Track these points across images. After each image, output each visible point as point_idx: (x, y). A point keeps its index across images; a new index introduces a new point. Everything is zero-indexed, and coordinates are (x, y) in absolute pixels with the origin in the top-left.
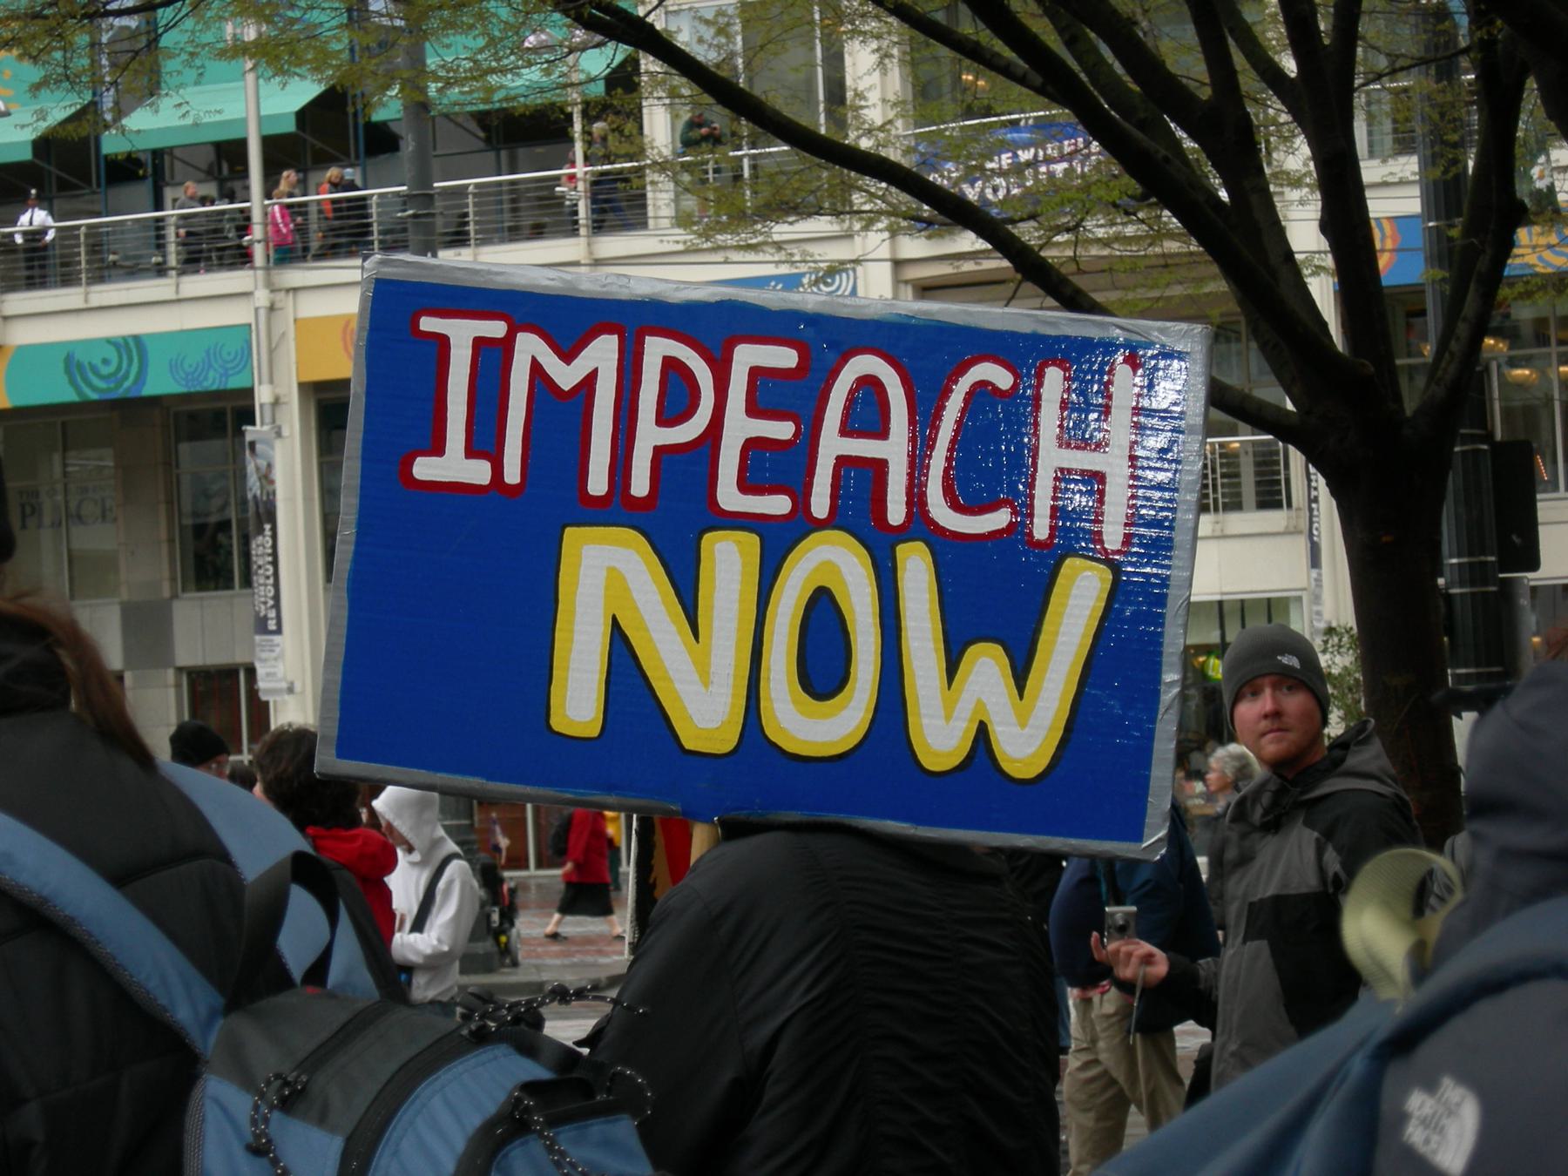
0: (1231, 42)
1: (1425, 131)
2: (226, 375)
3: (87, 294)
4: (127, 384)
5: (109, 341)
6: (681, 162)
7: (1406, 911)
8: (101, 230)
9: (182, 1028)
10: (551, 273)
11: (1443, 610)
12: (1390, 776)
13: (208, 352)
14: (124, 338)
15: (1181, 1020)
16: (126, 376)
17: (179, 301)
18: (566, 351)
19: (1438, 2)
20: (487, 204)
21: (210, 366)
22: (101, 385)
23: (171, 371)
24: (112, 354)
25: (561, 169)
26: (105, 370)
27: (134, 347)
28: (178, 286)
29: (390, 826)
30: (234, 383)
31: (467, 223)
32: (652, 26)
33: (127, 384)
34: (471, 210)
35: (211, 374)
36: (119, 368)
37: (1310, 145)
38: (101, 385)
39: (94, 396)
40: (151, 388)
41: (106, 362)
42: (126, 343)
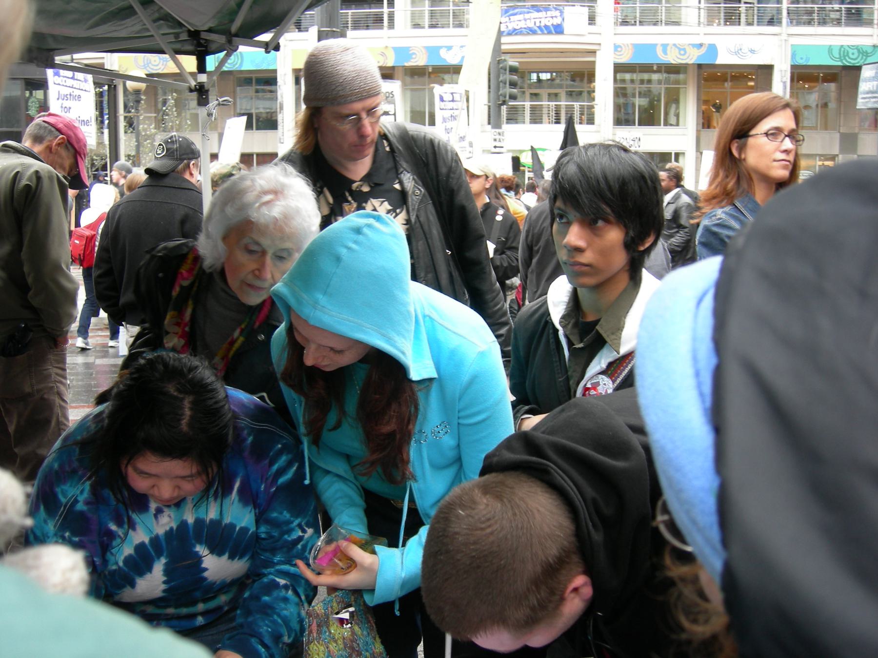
1: (257, 184)
2: (269, 65)
4: (237, 66)
6: (670, 4)
9: (744, 112)
10: (62, 47)
11: (647, 245)
12: (712, 208)
16: (236, 64)
19: (3, 269)
20: (345, 18)
23: (829, 52)
29: (566, 123)
30: (271, 68)
31: (348, 24)
33: (237, 66)
34: (350, 20)
35: (264, 65)
36: (234, 62)
37: (383, 643)
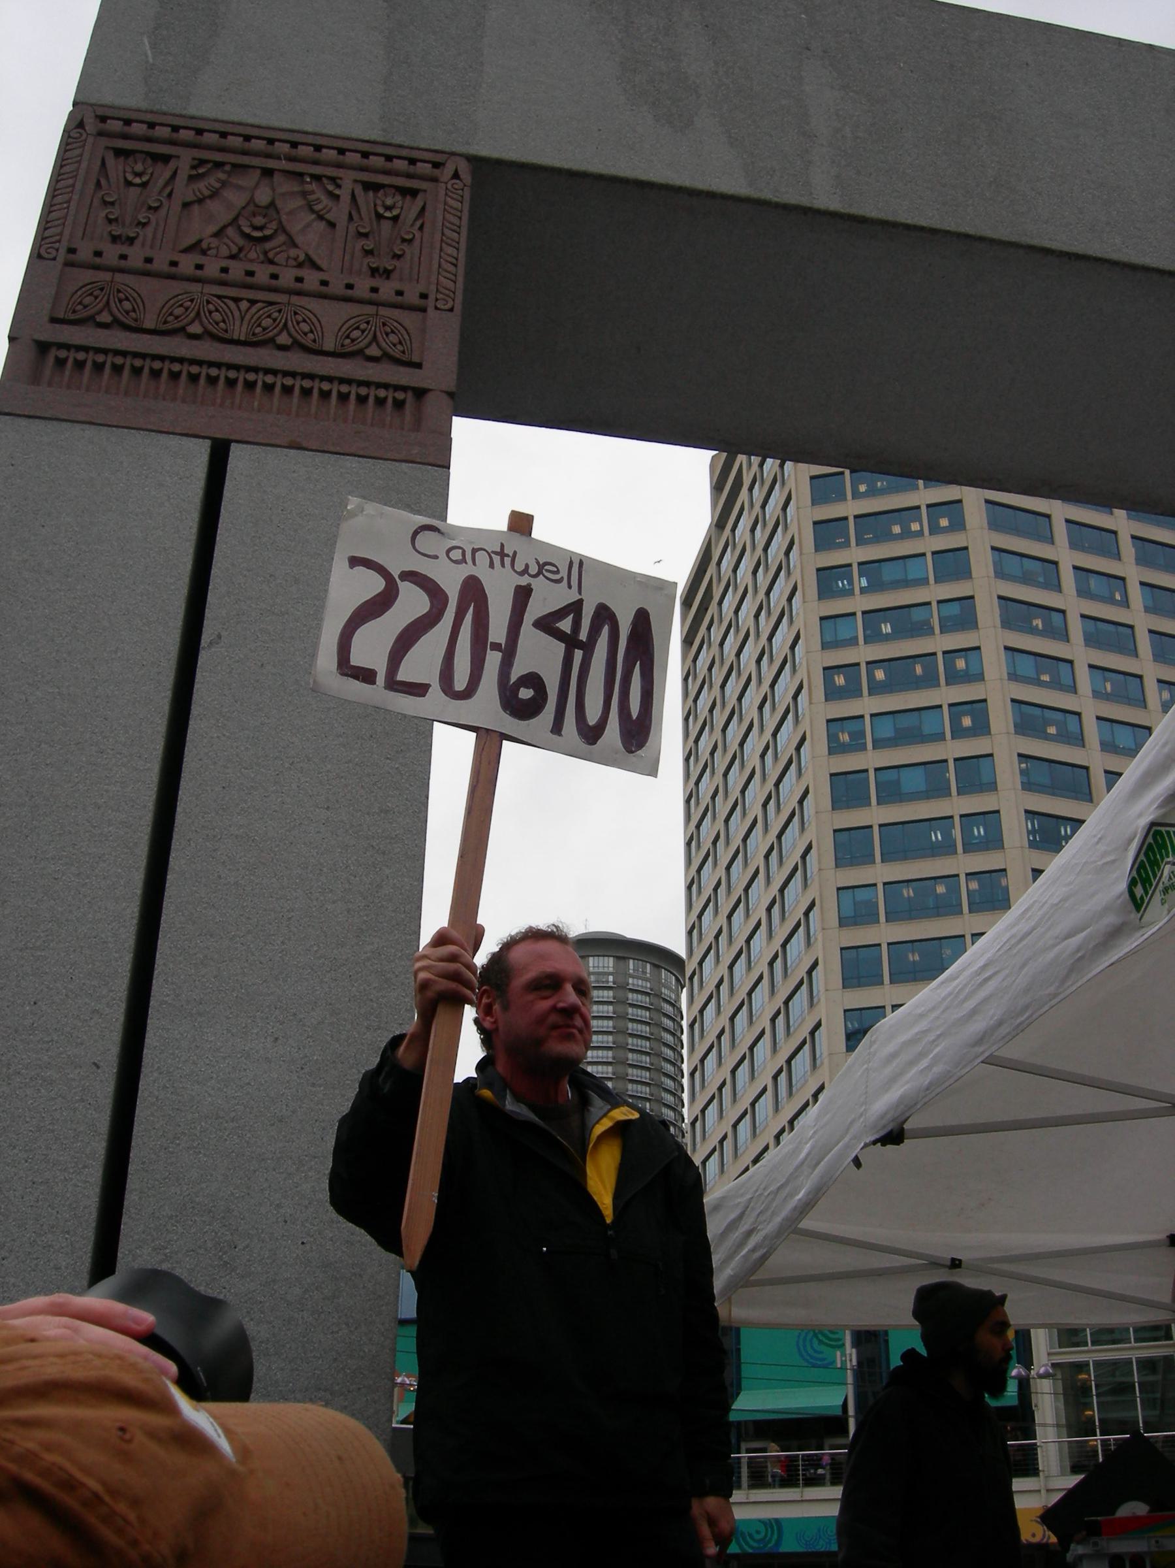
0: (472, 608)
3: (748, 1494)
5: (760, 1521)
7: (583, 559)
8: (758, 1460)
13: (819, 1530)
14: (769, 1520)
15: (961, 723)
17: (802, 1501)
18: (402, 676)
21: (820, 1537)
22: (755, 1545)
24: (762, 1529)
25: (949, 780)
26: (757, 1537)
27: (776, 1525)
28: (802, 1492)
32: (749, 454)
35: (821, 1542)
36: (766, 1536)
38: (755, 1545)
39: (750, 1551)
40: (784, 1548)
41: (758, 1532)
42: (771, 1524)
